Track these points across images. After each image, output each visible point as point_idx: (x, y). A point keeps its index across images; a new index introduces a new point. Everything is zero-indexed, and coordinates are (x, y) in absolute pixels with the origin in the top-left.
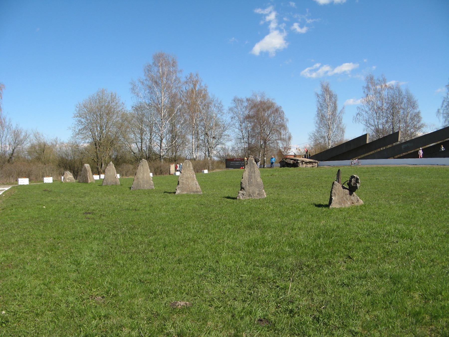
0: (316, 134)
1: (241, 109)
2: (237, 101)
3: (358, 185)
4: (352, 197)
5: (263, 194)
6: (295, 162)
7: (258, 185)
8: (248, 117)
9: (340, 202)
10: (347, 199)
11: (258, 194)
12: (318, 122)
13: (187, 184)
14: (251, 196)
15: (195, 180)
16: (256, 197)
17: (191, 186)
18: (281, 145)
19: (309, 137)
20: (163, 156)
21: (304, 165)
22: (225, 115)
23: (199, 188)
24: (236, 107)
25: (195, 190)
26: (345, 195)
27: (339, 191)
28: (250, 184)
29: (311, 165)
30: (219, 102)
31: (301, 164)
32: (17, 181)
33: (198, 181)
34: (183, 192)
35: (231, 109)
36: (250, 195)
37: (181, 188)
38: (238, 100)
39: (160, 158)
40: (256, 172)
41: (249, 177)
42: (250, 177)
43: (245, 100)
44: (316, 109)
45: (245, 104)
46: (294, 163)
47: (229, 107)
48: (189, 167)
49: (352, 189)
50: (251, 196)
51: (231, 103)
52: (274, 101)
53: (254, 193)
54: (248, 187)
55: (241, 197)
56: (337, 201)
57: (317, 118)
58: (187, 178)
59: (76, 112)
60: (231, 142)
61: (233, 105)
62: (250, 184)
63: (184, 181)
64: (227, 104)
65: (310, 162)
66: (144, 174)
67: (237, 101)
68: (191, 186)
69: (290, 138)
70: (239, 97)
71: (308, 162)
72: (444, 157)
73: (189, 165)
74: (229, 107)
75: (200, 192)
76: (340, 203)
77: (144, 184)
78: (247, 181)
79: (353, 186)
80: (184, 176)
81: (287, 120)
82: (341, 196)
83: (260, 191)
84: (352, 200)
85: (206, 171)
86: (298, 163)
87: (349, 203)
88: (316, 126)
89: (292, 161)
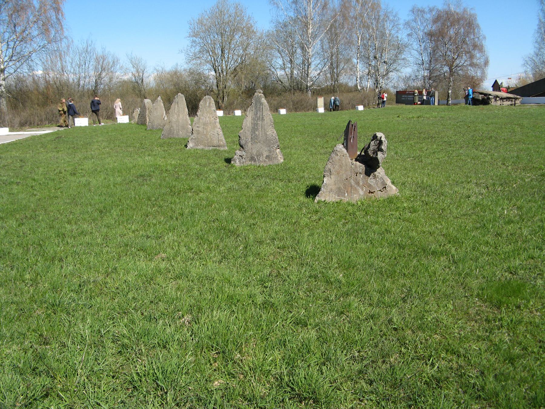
0: (534, 58)
1: (422, 23)
2: (418, 12)
3: (380, 155)
4: (371, 180)
5: (276, 158)
6: (486, 98)
7: (268, 142)
8: (430, 35)
9: (339, 189)
10: (358, 183)
11: (268, 157)
12: (539, 40)
13: (205, 133)
14: (255, 161)
15: (216, 127)
16: (263, 162)
17: (210, 136)
18: (472, 72)
19: (523, 62)
20: (310, 87)
21: (499, 103)
22: (400, 32)
23: (222, 140)
24: (415, 20)
25: (215, 142)
26: (354, 176)
27: (341, 166)
28: (254, 139)
29: (509, 103)
30: (394, 14)
31: (493, 100)
32: (233, 112)
33: (223, 129)
34: (197, 145)
35: (407, 24)
36: (252, 159)
37: (195, 139)
38: (419, 10)
39: (307, 89)
40: (265, 118)
41: (253, 128)
42: (255, 128)
43: (427, 10)
44: (537, 22)
45: (428, 16)
46: (483, 99)
47: (405, 20)
48: (210, 106)
49: (370, 164)
50: (255, 161)
51: (408, 15)
52: (472, 12)
53: (259, 155)
54: (250, 144)
55: (237, 161)
56: (334, 188)
57: (537, 35)
58: (205, 124)
59: (190, 31)
60: (408, 71)
61: (412, 17)
62: (254, 139)
63: (200, 129)
64: (404, 16)
65: (508, 99)
66: (179, 115)
67: (418, 12)
68: (210, 136)
69: (486, 63)
70: (419, 6)
71: (504, 98)
72: (81, 127)
73: (210, 103)
74: (405, 20)
75: (224, 146)
76: (339, 192)
77: (179, 129)
78: (249, 134)
79: (372, 158)
80: (201, 121)
81: (485, 38)
82: (344, 177)
83: (270, 151)
84: (370, 186)
85: (361, 108)
86: (489, 99)
87: (361, 193)
88: (535, 47)
89: (481, 96)
